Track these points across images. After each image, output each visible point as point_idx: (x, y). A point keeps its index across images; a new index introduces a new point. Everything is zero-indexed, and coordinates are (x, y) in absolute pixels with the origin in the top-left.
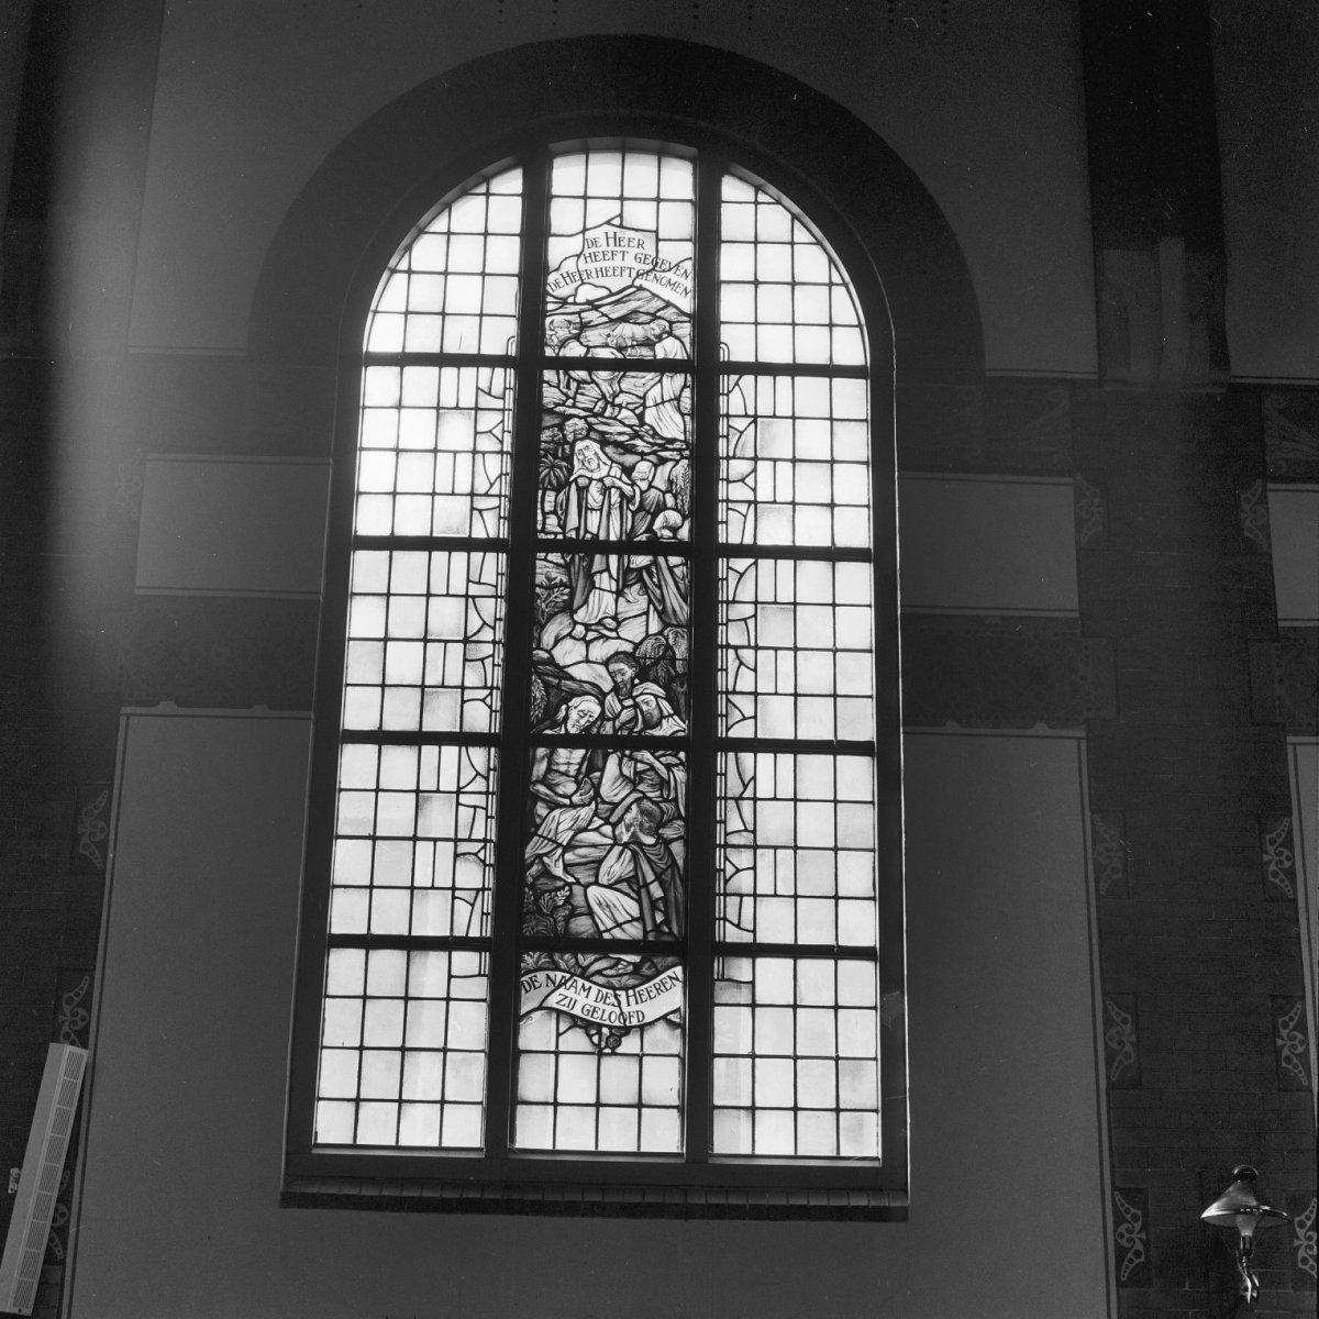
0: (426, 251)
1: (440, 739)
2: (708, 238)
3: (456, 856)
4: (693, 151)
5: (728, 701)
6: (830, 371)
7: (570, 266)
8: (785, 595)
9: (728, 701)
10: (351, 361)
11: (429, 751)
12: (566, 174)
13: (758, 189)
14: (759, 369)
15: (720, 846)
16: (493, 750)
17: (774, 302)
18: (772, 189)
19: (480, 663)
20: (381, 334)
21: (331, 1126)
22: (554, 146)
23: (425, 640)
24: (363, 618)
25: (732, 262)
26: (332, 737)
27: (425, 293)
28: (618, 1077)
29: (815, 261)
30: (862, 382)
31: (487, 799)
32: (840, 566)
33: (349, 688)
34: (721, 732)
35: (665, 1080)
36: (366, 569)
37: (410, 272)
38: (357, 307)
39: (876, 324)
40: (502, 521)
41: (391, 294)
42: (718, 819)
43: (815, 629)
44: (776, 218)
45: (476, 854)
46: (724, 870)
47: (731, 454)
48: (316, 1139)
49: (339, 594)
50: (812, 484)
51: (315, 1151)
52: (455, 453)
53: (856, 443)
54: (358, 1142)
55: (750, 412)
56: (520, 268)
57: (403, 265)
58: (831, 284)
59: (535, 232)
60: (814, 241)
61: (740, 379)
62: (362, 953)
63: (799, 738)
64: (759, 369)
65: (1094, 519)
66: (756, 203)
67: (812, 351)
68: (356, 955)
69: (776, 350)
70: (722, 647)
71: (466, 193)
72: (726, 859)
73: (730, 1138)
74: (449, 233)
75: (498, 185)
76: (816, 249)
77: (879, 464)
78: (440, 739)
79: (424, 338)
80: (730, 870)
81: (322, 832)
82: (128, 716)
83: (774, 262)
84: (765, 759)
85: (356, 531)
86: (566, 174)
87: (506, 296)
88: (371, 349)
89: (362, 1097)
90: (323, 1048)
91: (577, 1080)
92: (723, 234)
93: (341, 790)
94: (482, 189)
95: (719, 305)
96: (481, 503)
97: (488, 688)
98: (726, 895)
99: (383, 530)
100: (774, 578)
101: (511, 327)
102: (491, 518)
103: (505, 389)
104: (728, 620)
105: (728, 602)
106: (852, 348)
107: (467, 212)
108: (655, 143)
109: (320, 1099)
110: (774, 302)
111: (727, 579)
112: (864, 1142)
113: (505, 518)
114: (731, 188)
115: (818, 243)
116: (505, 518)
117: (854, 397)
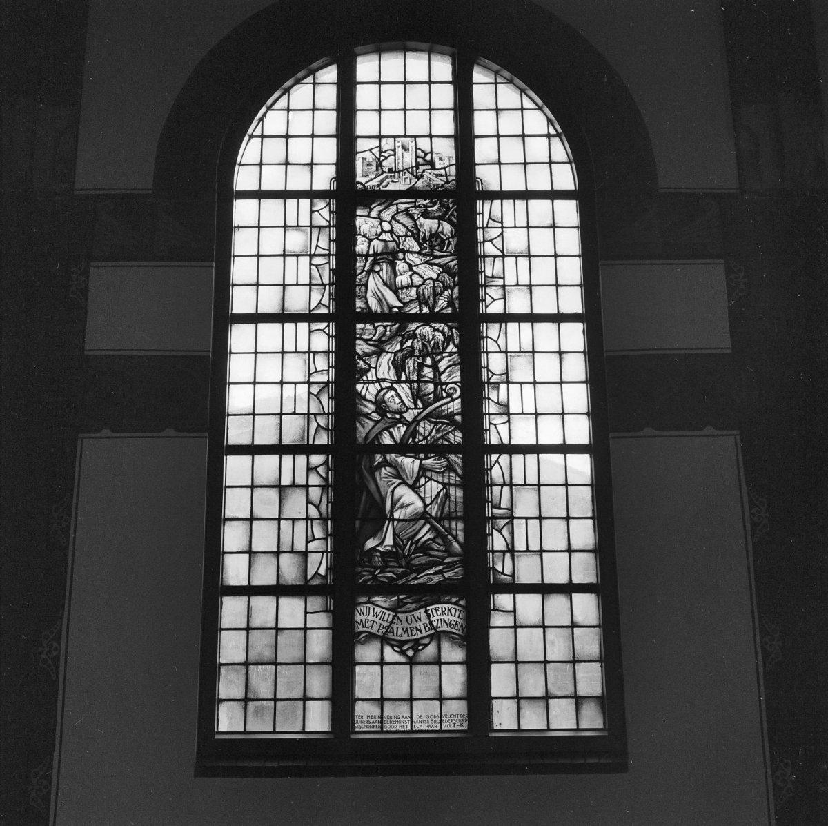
0: (273, 121)
1: (298, 195)
2: (464, 109)
3: (310, 332)
4: (450, 49)
8: (524, 280)
10: (227, 195)
11: (292, 202)
12: (366, 67)
13: (496, 73)
14: (502, 195)
15: (482, 286)
16: (330, 456)
18: (506, 73)
19: (318, 370)
20: (244, 179)
21: (228, 721)
22: (357, 50)
23: (284, 255)
25: (483, 123)
26: (220, 449)
28: (424, 681)
29: (537, 121)
30: (587, 456)
31: (328, 417)
32: (563, 325)
33: (227, 489)
34: (482, 310)
35: (454, 680)
37: (262, 137)
38: (229, 163)
39: (579, 159)
40: (332, 243)
41: (249, 151)
42: (478, 211)
43: (547, 367)
44: (509, 95)
45: (323, 330)
46: (485, 300)
47: (485, 226)
50: (548, 398)
51: (217, 737)
52: (297, 284)
54: (247, 730)
55: (503, 349)
57: (258, 132)
60: (536, 107)
61: (499, 457)
62: (256, 201)
63: (546, 581)
64: (502, 195)
65: (763, 522)
66: (496, 83)
67: (539, 181)
68: (249, 328)
69: (513, 181)
70: (481, 256)
71: (298, 82)
72: (486, 293)
73: (503, 718)
76: (538, 113)
78: (298, 195)
79: (273, 180)
80: (489, 300)
82: (83, 438)
83: (510, 123)
84: (508, 204)
86: (366, 67)
88: (234, 312)
89: (250, 484)
90: (228, 415)
91: (397, 682)
92: (475, 105)
93: (234, 285)
94: (310, 79)
95: (473, 100)
96: (316, 261)
97: (326, 414)
99: (245, 440)
100: (518, 335)
101: (331, 171)
102: (325, 213)
105: (483, 228)
106: (566, 179)
107: (301, 94)
108: (426, 45)
109: (230, 383)
110: (512, 151)
111: (489, 430)
113: (333, 241)
114: (478, 75)
115: (540, 109)
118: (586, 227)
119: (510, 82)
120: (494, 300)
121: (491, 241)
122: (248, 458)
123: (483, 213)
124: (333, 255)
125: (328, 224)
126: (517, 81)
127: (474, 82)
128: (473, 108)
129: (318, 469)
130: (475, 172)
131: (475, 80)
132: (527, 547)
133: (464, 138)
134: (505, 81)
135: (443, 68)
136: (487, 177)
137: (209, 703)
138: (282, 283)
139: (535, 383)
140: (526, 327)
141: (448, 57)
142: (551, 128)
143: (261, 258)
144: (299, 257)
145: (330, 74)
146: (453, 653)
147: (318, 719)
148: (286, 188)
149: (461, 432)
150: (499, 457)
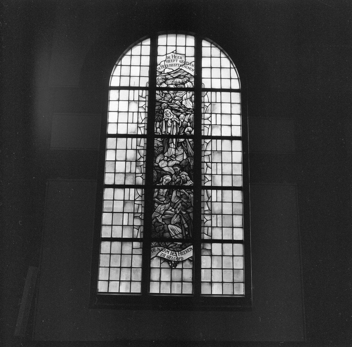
0: (125, 60)
2: (198, 56)
5: (204, 176)
6: (230, 90)
7: (163, 64)
8: (219, 123)
9: (204, 176)
12: (162, 40)
13: (211, 43)
15: (203, 214)
16: (143, 189)
17: (216, 73)
20: (114, 82)
21: (102, 287)
24: (110, 156)
25: (205, 62)
27: (125, 71)
29: (226, 62)
33: (109, 112)
34: (203, 184)
36: (110, 142)
37: (121, 65)
38: (108, 75)
39: (242, 79)
41: (117, 71)
44: (216, 51)
45: (139, 217)
46: (204, 220)
48: (98, 291)
49: (103, 149)
50: (226, 120)
53: (237, 109)
56: (150, 64)
58: (230, 68)
59: (154, 55)
61: (207, 93)
66: (211, 47)
69: (216, 85)
70: (203, 162)
72: (204, 217)
74: (131, 55)
75: (144, 43)
77: (243, 114)
78: (130, 187)
79: (125, 82)
81: (99, 211)
83: (216, 62)
85: (108, 133)
86: (162, 40)
87: (146, 71)
94: (140, 44)
96: (140, 125)
98: (204, 227)
101: (147, 79)
102: (142, 129)
103: (146, 96)
104: (204, 155)
106: (236, 85)
107: (136, 50)
109: (106, 173)
110: (216, 73)
112: (240, 291)
114: (205, 43)
116: (146, 144)
117: (236, 97)
118: (243, 104)
119: (217, 47)
120: (207, 220)
121: (209, 181)
122: (113, 237)
123: (204, 168)
124: (147, 101)
125: (144, 111)
126: (219, 46)
127: (203, 56)
128: (202, 56)
129: (143, 107)
130: (202, 81)
131: (203, 45)
132: (217, 225)
133: (198, 68)
134: (215, 46)
135: (191, 41)
136: (206, 84)
137: (95, 279)
138: (122, 225)
139: (222, 163)
140: (219, 141)
141: (193, 37)
142: (232, 65)
143: (122, 67)
144: (127, 225)
145: (148, 42)
146: (188, 264)
147: (137, 288)
148: (125, 183)
149: (194, 195)
150: (207, 93)
